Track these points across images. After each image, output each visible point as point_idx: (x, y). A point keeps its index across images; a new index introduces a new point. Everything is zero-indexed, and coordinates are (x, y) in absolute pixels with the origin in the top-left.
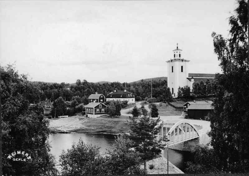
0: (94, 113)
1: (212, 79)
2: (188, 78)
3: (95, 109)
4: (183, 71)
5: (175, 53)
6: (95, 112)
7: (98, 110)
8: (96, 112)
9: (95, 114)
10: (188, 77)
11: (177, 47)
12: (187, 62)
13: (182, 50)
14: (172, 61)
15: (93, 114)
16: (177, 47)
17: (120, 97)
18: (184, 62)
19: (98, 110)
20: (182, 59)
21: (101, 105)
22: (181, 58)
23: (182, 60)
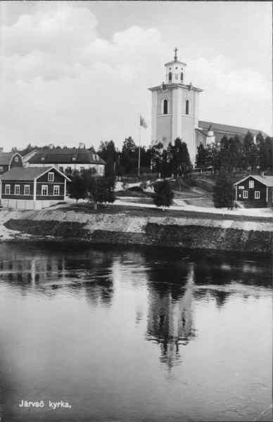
0: (35, 195)
1: (36, 168)
2: (196, 129)
3: (37, 185)
4: (190, 113)
5: (171, 71)
6: (64, 185)
7: (44, 187)
8: (23, 193)
9: (38, 198)
10: (197, 128)
11: (176, 58)
12: (196, 93)
13: (185, 65)
14: (164, 86)
15: (31, 198)
16: (176, 58)
17: (72, 162)
18: (191, 92)
19: (44, 187)
20: (189, 84)
21: (53, 173)
22: (186, 82)
23: (189, 87)
